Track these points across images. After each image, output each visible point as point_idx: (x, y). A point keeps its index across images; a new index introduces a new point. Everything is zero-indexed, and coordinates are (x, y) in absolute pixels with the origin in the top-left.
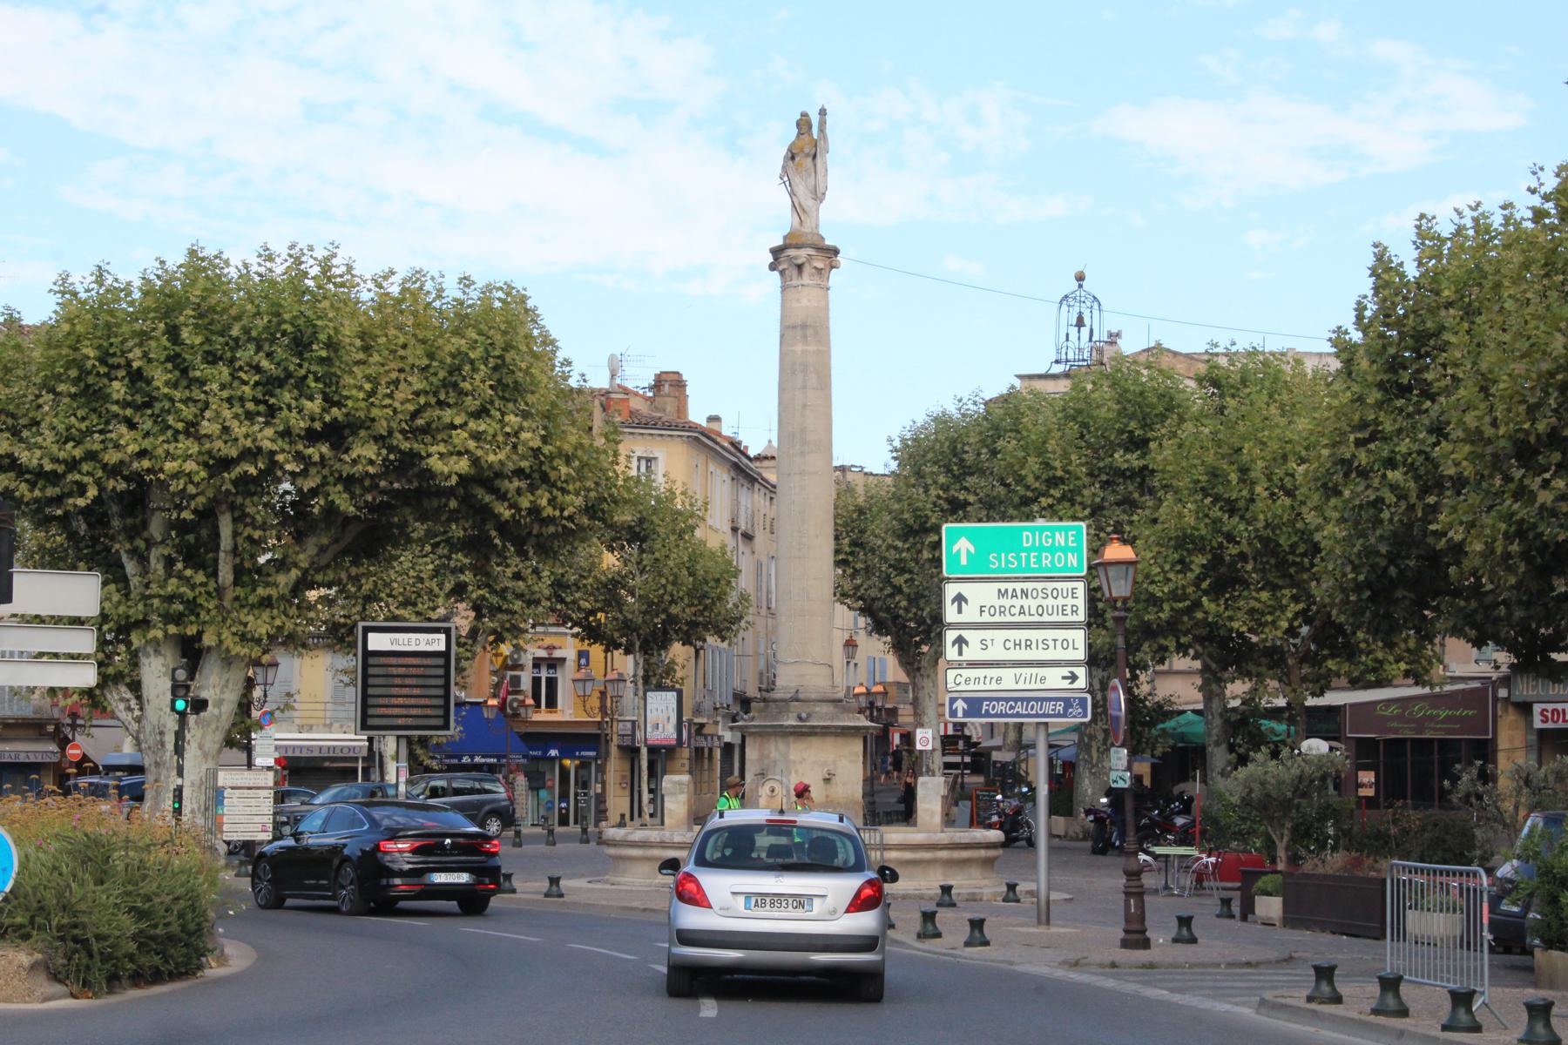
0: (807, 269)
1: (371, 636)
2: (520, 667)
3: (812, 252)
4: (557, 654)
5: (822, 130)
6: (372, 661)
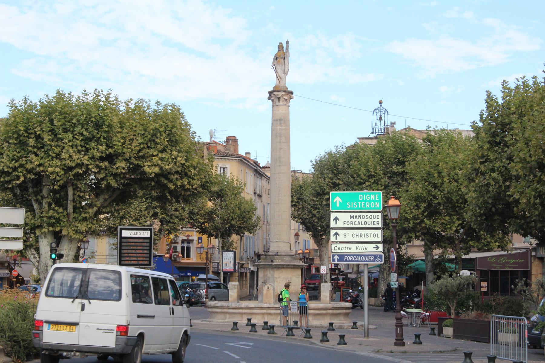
0: (281, 99)
1: (123, 231)
2: (177, 243)
3: (283, 93)
4: (190, 238)
5: (287, 49)
6: (123, 240)
